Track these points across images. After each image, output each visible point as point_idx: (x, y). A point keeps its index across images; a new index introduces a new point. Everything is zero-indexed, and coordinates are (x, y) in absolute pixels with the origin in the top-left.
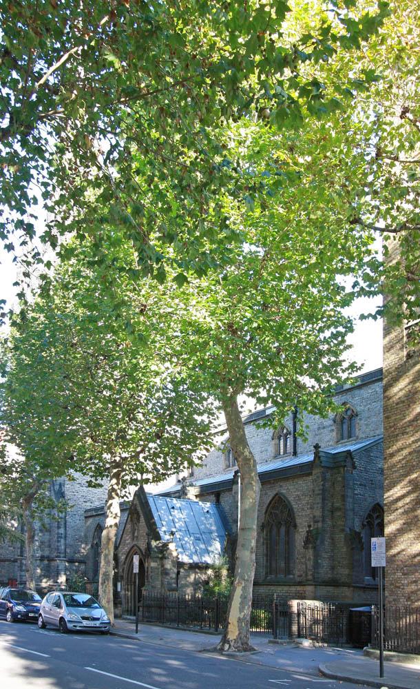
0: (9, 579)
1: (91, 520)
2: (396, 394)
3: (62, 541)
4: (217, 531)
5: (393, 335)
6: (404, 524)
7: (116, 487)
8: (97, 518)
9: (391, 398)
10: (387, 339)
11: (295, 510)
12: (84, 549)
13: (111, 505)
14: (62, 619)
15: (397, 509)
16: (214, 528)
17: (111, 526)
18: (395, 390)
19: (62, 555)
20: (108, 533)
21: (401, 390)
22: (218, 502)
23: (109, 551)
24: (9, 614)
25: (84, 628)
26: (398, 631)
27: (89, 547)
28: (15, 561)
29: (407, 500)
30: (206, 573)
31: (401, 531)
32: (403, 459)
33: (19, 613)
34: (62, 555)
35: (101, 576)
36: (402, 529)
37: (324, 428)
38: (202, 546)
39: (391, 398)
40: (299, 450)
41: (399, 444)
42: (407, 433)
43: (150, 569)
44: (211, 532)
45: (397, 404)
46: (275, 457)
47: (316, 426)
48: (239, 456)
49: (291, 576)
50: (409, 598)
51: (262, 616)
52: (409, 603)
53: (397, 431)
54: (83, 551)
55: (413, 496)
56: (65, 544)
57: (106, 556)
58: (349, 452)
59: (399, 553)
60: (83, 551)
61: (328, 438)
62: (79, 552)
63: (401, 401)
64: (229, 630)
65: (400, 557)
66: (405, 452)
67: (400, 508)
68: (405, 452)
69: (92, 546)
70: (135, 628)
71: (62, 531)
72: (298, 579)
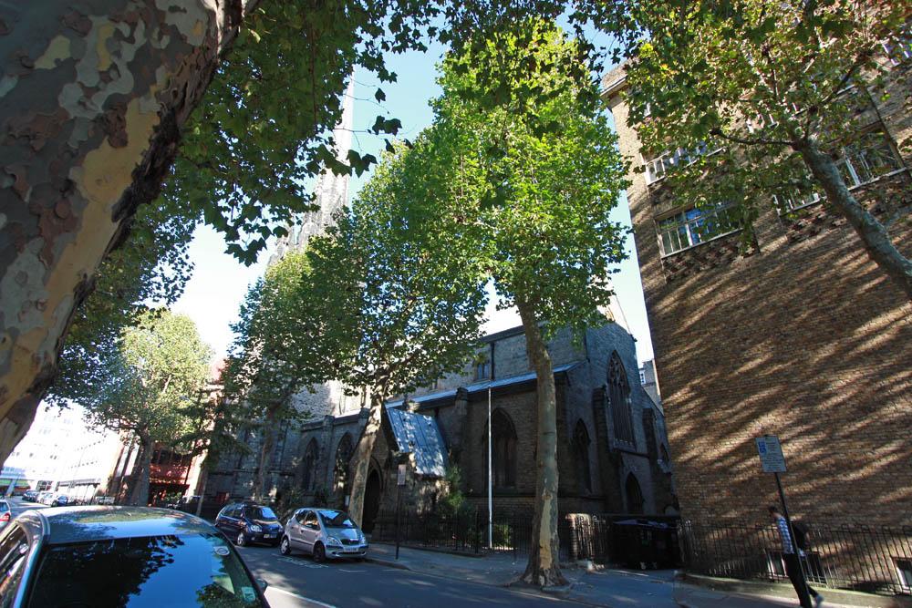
0: (217, 493)
1: (306, 434)
2: (661, 310)
3: (280, 454)
4: (439, 443)
5: (650, 264)
6: (692, 429)
7: (380, 393)
8: (312, 432)
9: (656, 314)
10: (644, 268)
11: (516, 423)
12: (296, 462)
13: (374, 411)
14: (319, 543)
15: (680, 415)
16: (436, 440)
17: (371, 433)
18: (660, 307)
19: (277, 468)
20: (369, 441)
21: (666, 307)
22: (436, 417)
23: (366, 461)
24: (242, 535)
25: (342, 556)
26: (704, 549)
27: (301, 459)
28: (231, 474)
29: (692, 405)
30: (434, 485)
31: (689, 437)
32: (679, 367)
33: (253, 534)
34: (277, 468)
35: (354, 489)
36: (690, 434)
37: (518, 357)
38: (429, 457)
39: (656, 314)
40: (496, 375)
41: (673, 353)
42: (681, 344)
43: (389, 481)
44: (434, 445)
45: (664, 319)
46: (475, 381)
47: (512, 356)
48: (538, 358)
49: (512, 487)
50: (712, 510)
51: (506, 530)
52: (713, 515)
53: (668, 343)
54: (294, 464)
55: (697, 401)
56: (282, 456)
57: (363, 465)
58: (565, 372)
59: (690, 460)
60: (294, 464)
61: (522, 365)
62: (291, 464)
63: (667, 316)
64: (541, 556)
65: (693, 464)
66: (680, 361)
67: (684, 413)
68: (680, 361)
69: (304, 459)
70: (395, 552)
71: (281, 444)
72: (521, 490)
